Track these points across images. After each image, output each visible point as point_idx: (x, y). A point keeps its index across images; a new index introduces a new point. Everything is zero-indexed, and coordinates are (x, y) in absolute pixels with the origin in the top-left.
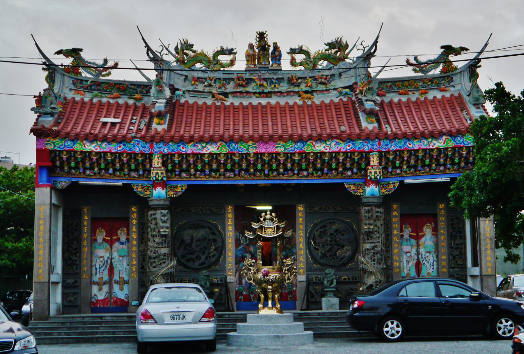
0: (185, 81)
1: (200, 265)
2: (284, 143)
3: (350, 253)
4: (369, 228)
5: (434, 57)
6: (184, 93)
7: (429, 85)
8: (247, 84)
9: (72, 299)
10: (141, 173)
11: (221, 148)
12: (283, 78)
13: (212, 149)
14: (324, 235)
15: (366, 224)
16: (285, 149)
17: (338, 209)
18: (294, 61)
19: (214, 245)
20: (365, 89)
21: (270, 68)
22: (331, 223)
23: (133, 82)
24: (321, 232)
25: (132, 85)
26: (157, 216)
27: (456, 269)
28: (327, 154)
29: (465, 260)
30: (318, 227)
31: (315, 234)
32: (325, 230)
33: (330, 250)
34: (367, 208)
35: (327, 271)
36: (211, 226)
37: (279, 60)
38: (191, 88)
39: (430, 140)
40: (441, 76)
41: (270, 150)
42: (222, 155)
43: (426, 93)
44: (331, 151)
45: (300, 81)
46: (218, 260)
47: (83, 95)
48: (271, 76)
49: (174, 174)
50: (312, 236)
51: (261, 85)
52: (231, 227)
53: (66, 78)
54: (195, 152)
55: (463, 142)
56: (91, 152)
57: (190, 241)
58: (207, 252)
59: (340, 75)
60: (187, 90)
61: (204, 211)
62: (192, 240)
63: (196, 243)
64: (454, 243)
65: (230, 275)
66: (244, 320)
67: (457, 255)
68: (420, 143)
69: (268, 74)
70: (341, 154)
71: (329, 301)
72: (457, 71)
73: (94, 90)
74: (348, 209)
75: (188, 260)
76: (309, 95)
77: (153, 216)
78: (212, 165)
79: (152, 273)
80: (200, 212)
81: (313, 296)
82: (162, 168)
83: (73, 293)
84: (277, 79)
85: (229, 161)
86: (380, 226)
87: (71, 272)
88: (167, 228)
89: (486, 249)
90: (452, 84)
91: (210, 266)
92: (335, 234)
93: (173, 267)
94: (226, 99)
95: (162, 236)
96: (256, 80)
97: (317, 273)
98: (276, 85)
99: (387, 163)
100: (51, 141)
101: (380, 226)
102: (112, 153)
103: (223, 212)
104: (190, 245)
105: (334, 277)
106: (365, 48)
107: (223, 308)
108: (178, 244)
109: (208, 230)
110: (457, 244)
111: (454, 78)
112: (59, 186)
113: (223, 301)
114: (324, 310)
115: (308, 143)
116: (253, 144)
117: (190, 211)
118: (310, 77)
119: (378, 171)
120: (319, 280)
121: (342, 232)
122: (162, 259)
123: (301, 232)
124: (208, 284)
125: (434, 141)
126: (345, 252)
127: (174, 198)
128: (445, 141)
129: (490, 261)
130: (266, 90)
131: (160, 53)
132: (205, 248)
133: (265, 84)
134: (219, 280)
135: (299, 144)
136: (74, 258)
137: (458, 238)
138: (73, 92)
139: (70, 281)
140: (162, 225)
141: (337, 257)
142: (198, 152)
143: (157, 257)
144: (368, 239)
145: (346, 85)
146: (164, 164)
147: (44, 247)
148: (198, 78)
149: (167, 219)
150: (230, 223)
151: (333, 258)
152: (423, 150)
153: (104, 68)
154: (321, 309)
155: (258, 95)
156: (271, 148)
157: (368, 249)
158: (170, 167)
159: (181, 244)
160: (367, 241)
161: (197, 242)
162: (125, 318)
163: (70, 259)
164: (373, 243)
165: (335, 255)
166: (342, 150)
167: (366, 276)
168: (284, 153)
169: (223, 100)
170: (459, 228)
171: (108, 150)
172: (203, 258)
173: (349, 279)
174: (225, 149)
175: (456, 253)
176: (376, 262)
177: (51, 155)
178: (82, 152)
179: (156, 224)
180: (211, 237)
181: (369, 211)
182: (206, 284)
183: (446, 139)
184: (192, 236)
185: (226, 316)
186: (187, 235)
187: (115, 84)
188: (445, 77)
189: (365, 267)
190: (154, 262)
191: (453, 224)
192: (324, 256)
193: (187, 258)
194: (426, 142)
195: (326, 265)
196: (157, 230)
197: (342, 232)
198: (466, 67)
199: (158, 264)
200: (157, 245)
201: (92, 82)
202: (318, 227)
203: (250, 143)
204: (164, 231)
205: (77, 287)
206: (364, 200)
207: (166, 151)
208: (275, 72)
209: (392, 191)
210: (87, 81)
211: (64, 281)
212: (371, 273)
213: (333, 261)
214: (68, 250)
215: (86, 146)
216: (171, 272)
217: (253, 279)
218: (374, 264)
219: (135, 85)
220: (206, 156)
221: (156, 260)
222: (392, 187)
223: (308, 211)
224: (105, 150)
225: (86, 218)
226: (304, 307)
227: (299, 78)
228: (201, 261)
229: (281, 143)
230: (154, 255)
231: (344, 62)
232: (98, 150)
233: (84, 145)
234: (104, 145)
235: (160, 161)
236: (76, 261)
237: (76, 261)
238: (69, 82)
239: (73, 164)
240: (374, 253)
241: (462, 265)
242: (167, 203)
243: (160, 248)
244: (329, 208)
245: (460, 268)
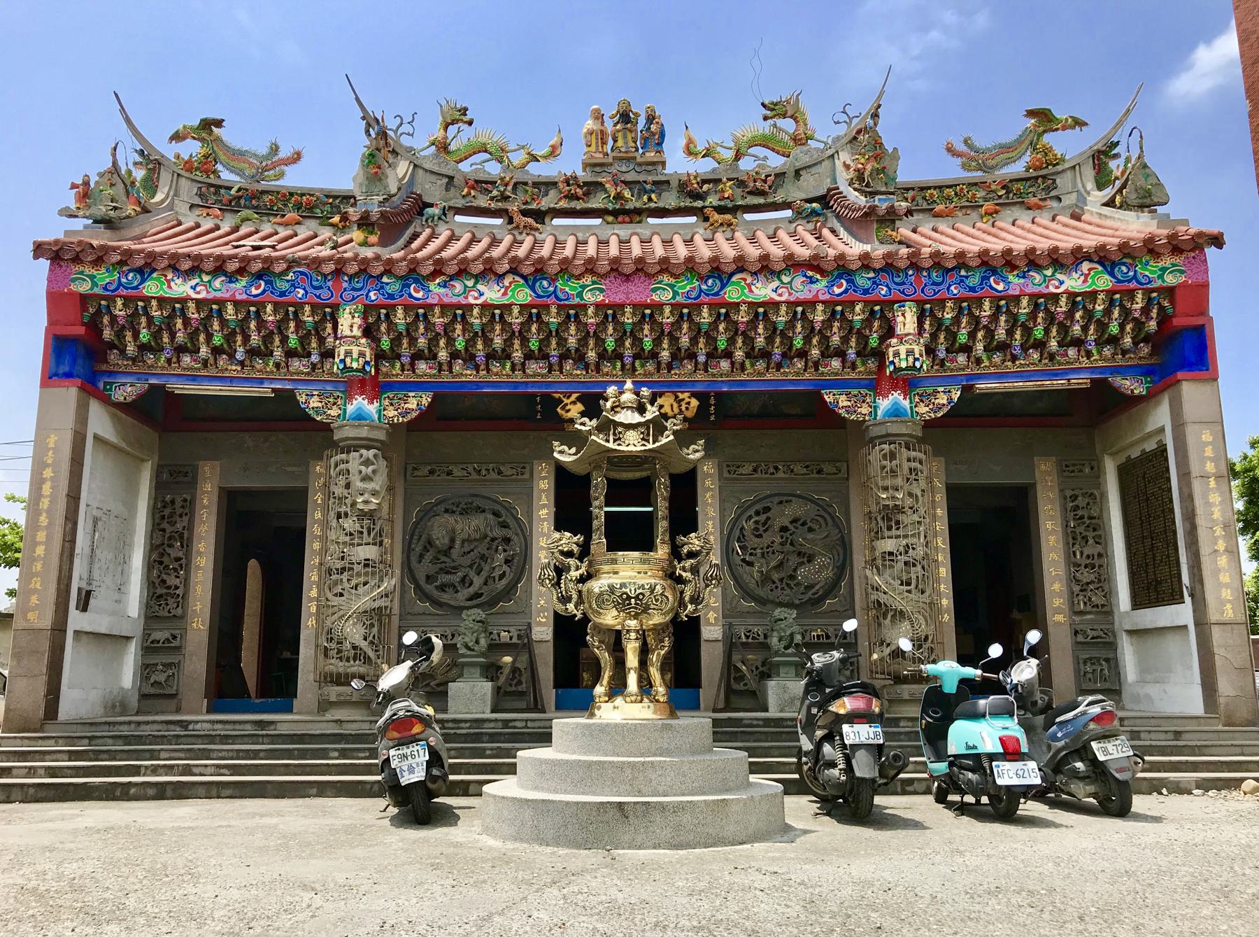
0: (447, 189)
1: (470, 599)
2: (672, 281)
3: (828, 574)
4: (893, 497)
5: (1008, 137)
6: (445, 214)
7: (1000, 197)
8: (587, 194)
9: (162, 678)
10: (315, 358)
11: (513, 291)
12: (668, 182)
13: (491, 293)
14: (765, 531)
15: (886, 489)
16: (675, 294)
17: (798, 468)
18: (692, 146)
19: (505, 551)
20: (869, 167)
21: (639, 160)
22: (781, 502)
23: (331, 191)
24: (756, 522)
25: (327, 196)
26: (350, 466)
27: (1089, 617)
28: (783, 308)
29: (1109, 594)
30: (752, 512)
31: (743, 528)
32: (768, 518)
33: (780, 566)
34: (886, 447)
35: (779, 613)
36: (497, 507)
37: (660, 144)
38: (460, 203)
39: (1049, 272)
40: (1028, 175)
41: (637, 298)
42: (516, 310)
43: (996, 212)
44: (792, 299)
45: (706, 187)
46: (512, 588)
47: (217, 217)
48: (641, 178)
49: (398, 365)
50: (737, 533)
51: (619, 197)
52: (545, 511)
53: (183, 181)
54: (446, 300)
55: (1135, 277)
56: (184, 301)
57: (446, 541)
58: (486, 568)
59: (797, 173)
60: (450, 208)
61: (484, 472)
62: (453, 540)
63: (462, 546)
64: (1082, 553)
65: (540, 624)
66: (545, 738)
67: (1092, 582)
68: (1022, 281)
69: (633, 173)
70: (820, 307)
71: (785, 689)
72: (1067, 165)
73: (246, 207)
74: (819, 472)
75: (442, 588)
76: (728, 217)
77: (342, 466)
78: (492, 340)
79: (331, 611)
80: (475, 476)
81: (741, 678)
82: (363, 341)
83: (164, 665)
84: (654, 183)
85: (534, 328)
86: (919, 494)
87: (161, 613)
88: (374, 493)
89: (1216, 551)
90: (1053, 193)
91: (492, 603)
92: (790, 527)
93: (387, 596)
94: (539, 226)
95: (362, 515)
96: (607, 186)
97: (751, 621)
98: (653, 196)
99: (934, 336)
100: (87, 272)
101: (919, 494)
102: (237, 304)
103: (526, 476)
104: (447, 552)
105: (796, 628)
106: (851, 119)
107: (523, 705)
108: (418, 549)
109: (491, 516)
110: (1088, 557)
111: (1058, 181)
112: (119, 395)
113: (523, 687)
114: (773, 713)
115: (734, 279)
116: (594, 283)
117: (449, 473)
118: (729, 180)
119: (917, 349)
120: (754, 638)
121: (810, 524)
122: (359, 575)
123: (710, 523)
124: (483, 642)
125: (1058, 276)
126: (817, 572)
127: (398, 424)
128: (1087, 276)
129: (1227, 586)
130: (630, 206)
131: (396, 132)
132: (483, 557)
133: (627, 194)
134: (515, 635)
135: (710, 282)
136: (172, 581)
137: (1091, 541)
138: (198, 211)
139: (160, 635)
140: (360, 484)
141: (798, 584)
142: (455, 300)
143: (344, 569)
144: (890, 528)
145: (811, 196)
146: (369, 332)
147: (49, 537)
148: (477, 182)
149: (374, 472)
150: (544, 501)
151: (788, 585)
152: (1032, 296)
153: (274, 160)
154: (767, 710)
155: (610, 219)
156: (637, 292)
157: (891, 554)
158: (385, 343)
159: (426, 549)
160: (887, 533)
161: (466, 544)
162: (248, 727)
163: (164, 581)
164: (906, 536)
165: (792, 577)
166: (822, 298)
167: (888, 621)
168: (672, 305)
169: (532, 229)
170: (1091, 518)
171: (227, 295)
172: (478, 581)
173: (828, 637)
174: (524, 295)
175: (1086, 576)
176: (913, 586)
177: (87, 311)
178: (162, 300)
179: (348, 486)
180: (498, 532)
181: (893, 456)
182: (477, 642)
183: (1090, 270)
184: (453, 531)
185: (518, 724)
186: (439, 530)
187: (291, 194)
188: (1037, 178)
189: (883, 598)
190: (336, 583)
191: (1076, 508)
192: (766, 579)
193: (438, 583)
194: (1038, 278)
195: (772, 602)
196: (348, 501)
197: (810, 524)
198: (1086, 156)
199: (346, 585)
200: (348, 539)
201: (239, 190)
202: (752, 512)
203: (588, 280)
204: (366, 502)
205: (178, 648)
206: (875, 431)
207: (373, 298)
208: (650, 168)
209: (945, 410)
210: (230, 188)
211: (146, 635)
212: (900, 615)
213: (788, 591)
214: (161, 563)
215: (172, 284)
216: (380, 608)
217: (575, 596)
218: (909, 592)
219: (335, 197)
220: (476, 311)
221: (345, 576)
222: (942, 399)
223: (726, 475)
224: (218, 294)
225: (208, 487)
226: (721, 705)
227: (705, 182)
228: (472, 590)
229: (666, 279)
230: (339, 565)
231: (805, 148)
232: (203, 295)
233: (169, 282)
234: (217, 283)
235: (358, 321)
236: (177, 588)
237: (177, 588)
238: (190, 190)
239: (144, 335)
240: (906, 563)
241: (1103, 606)
242: (381, 435)
243: (353, 545)
244: (776, 468)
245: (1097, 613)
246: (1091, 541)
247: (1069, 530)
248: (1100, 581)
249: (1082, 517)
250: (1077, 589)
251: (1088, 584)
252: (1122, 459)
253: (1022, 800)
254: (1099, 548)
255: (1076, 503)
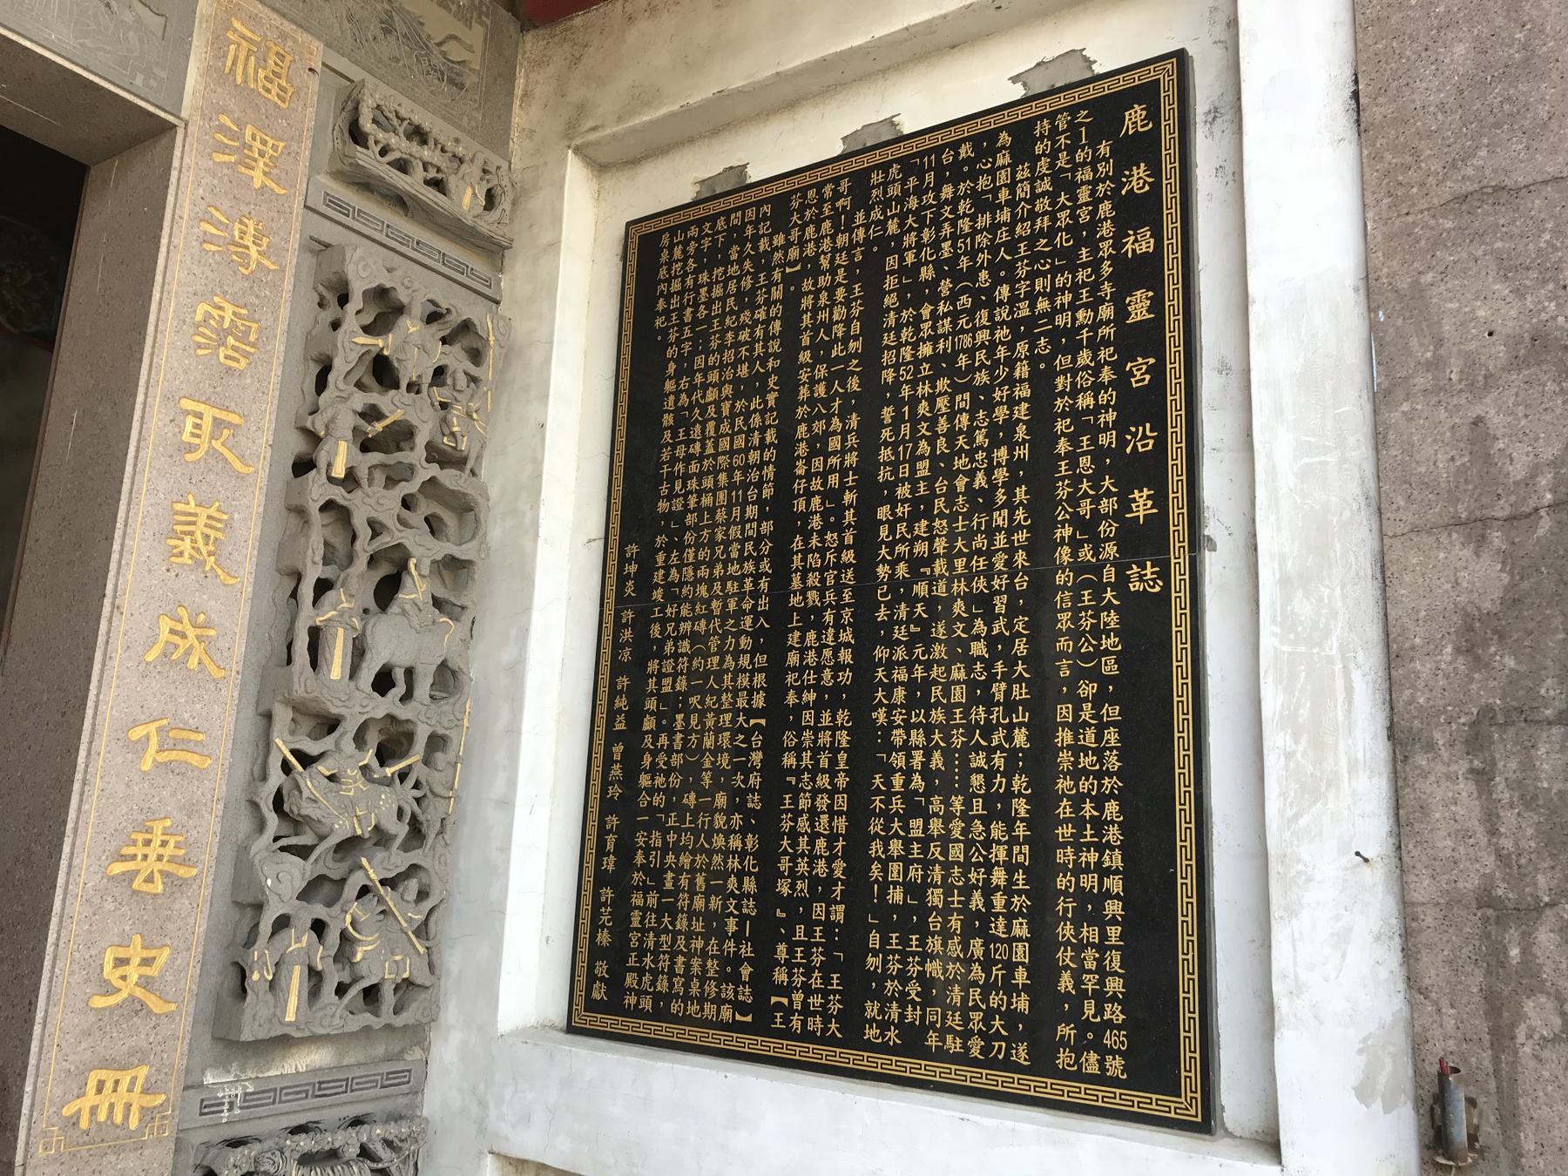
64: (359, 651)
67: (381, 837)
175: (349, 797)
246: (417, 589)
247: (317, 490)
248: (417, 831)
249: (401, 435)
250: (283, 880)
251: (349, 846)
252: (671, 185)
253: (1151, 294)
254: (445, 639)
255: (385, 343)
